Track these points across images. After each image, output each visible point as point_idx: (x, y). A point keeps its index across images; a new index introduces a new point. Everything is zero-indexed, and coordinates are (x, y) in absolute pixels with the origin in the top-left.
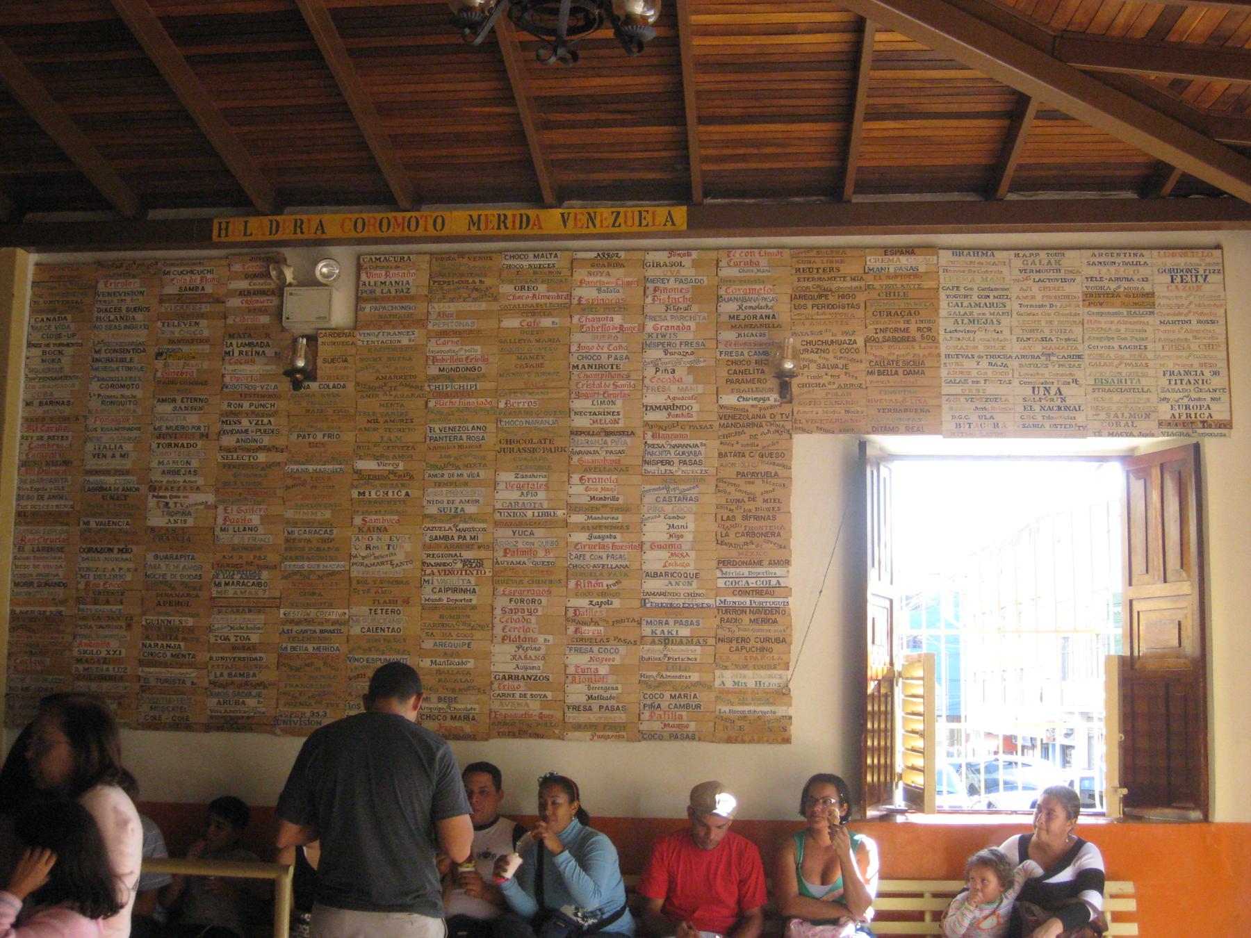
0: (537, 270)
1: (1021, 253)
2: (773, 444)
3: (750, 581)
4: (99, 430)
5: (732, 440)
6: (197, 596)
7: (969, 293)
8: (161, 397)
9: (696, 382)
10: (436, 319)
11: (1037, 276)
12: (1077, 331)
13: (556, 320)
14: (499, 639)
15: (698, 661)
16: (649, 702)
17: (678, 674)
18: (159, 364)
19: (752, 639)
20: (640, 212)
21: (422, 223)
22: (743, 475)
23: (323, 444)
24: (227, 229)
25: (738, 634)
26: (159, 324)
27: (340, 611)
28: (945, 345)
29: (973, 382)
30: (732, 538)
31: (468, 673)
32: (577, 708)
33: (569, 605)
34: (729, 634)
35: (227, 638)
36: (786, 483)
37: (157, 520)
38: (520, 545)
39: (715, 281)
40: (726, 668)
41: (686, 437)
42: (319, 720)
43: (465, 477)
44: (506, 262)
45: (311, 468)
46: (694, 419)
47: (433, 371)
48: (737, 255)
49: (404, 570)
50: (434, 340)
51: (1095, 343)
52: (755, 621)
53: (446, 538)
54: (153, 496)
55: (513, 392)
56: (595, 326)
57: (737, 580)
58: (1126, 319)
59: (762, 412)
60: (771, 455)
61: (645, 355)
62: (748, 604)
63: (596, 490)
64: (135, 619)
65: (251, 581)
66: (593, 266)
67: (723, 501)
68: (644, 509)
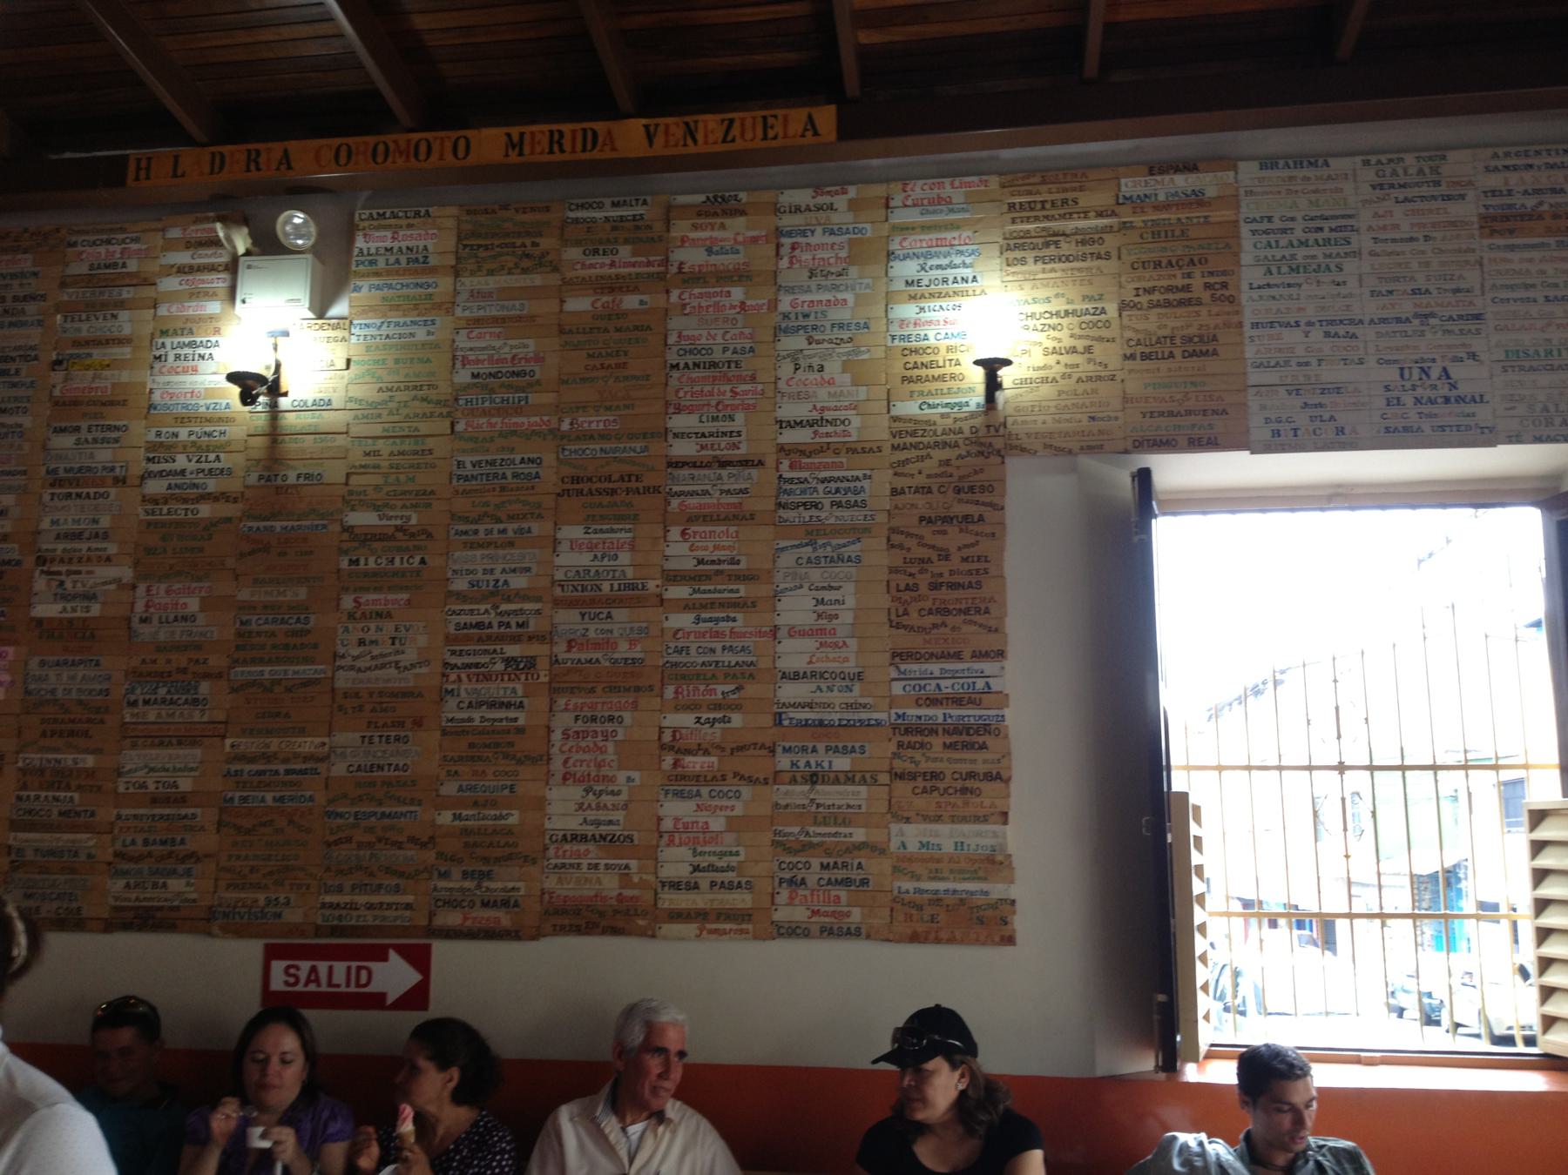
0: (617, 224)
1: (1373, 159)
2: (976, 472)
3: (943, 683)
7: (1290, 225)
8: (58, 425)
10: (467, 300)
11: (1401, 194)
12: (1472, 277)
13: (645, 298)
14: (558, 777)
15: (863, 810)
16: (787, 876)
17: (833, 830)
18: (57, 377)
19: (948, 774)
20: (765, 118)
22: (930, 521)
24: (148, 169)
25: (925, 766)
27: (318, 740)
28: (1252, 306)
29: (1300, 364)
30: (914, 619)
31: (509, 831)
32: (675, 885)
33: (666, 723)
34: (911, 767)
35: (144, 786)
36: (997, 534)
37: (47, 609)
38: (592, 634)
40: (908, 820)
41: (839, 466)
42: (278, 910)
43: (510, 534)
45: (278, 525)
46: (854, 438)
48: (918, 190)
49: (416, 675)
51: (1504, 295)
53: (479, 625)
55: (582, 407)
57: (923, 683)
58: (1555, 254)
59: (959, 424)
60: (971, 489)
61: (779, 346)
62: (940, 720)
63: (706, 549)
65: (184, 697)
66: (699, 215)
67: (899, 563)
68: (779, 577)
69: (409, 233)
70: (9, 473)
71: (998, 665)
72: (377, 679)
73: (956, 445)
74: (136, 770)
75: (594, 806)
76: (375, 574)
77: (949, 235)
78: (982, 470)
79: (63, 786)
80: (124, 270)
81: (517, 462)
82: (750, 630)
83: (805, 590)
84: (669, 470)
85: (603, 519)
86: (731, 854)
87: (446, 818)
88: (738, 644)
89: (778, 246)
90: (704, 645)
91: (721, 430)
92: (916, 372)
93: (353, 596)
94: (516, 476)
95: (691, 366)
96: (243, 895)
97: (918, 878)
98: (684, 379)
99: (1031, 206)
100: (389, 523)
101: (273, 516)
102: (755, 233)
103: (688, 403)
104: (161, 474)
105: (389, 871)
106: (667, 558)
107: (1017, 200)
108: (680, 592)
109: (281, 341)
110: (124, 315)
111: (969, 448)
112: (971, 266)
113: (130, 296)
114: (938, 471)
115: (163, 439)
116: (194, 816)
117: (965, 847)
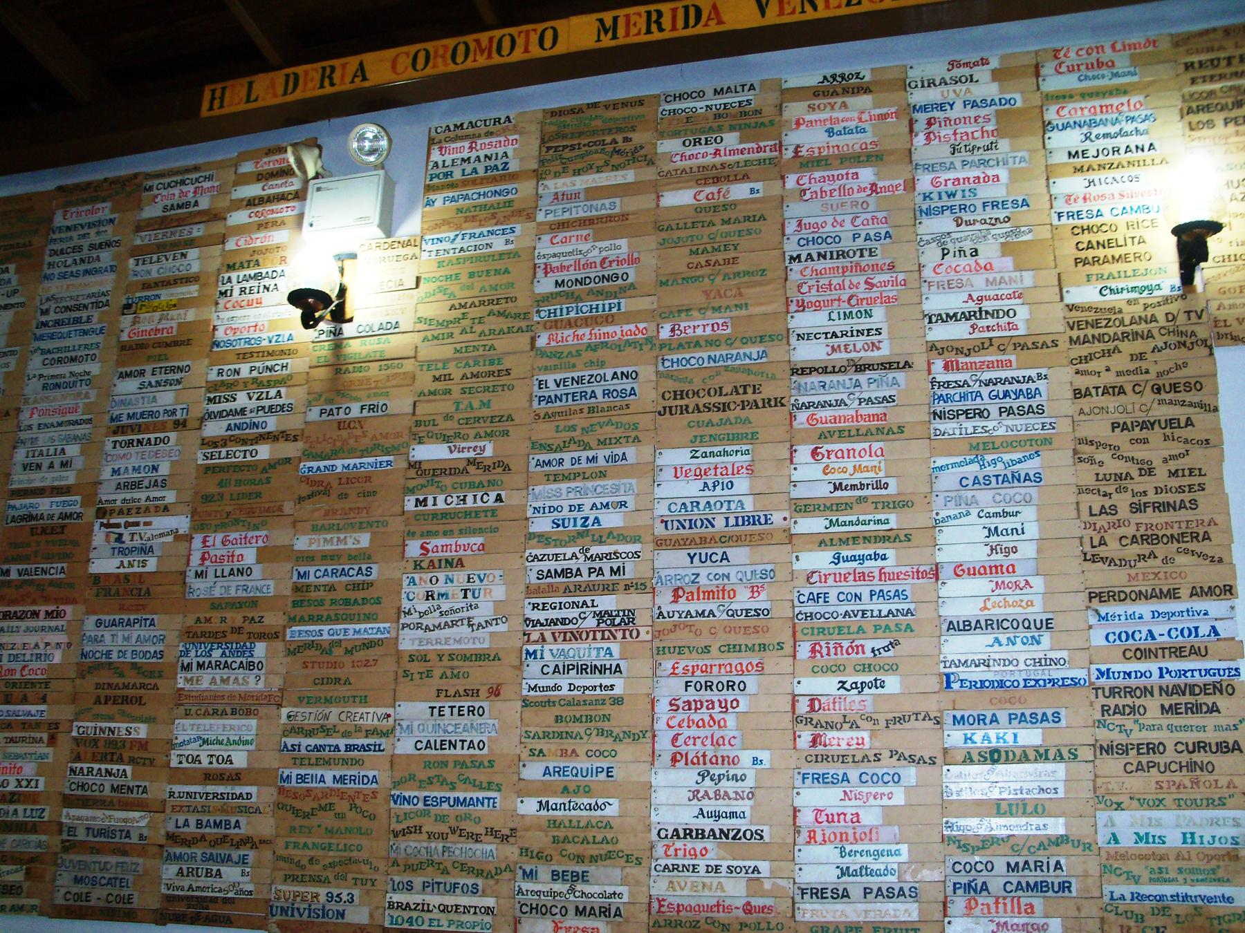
2: (1178, 367)
4: (35, 427)
5: (1093, 365)
6: (156, 687)
9: (1018, 268)
10: (551, 204)
13: (757, 186)
14: (667, 758)
16: (964, 880)
19: (1170, 746)
21: (520, 42)
23: (359, 421)
24: (222, 98)
25: (1138, 736)
26: (131, 261)
27: (381, 711)
30: (1113, 549)
31: (608, 826)
32: (818, 893)
33: (799, 690)
34: (1120, 738)
35: (196, 760)
37: (104, 564)
39: (1036, 100)
43: (601, 462)
44: (668, 107)
45: (339, 464)
47: (546, 285)
49: (492, 634)
50: (546, 238)
52: (1173, 710)
53: (564, 573)
54: (102, 524)
55: (685, 310)
56: (827, 188)
59: (1150, 312)
60: (1174, 387)
64: (61, 728)
65: (238, 660)
67: (1088, 479)
69: (487, 141)
70: (76, 423)
71: (1228, 603)
72: (447, 639)
73: (1150, 335)
74: (189, 742)
75: (712, 795)
76: (445, 514)
77: (1115, 101)
78: (1185, 365)
79: (115, 757)
80: (196, 208)
81: (609, 377)
82: (904, 569)
83: (973, 518)
84: (794, 378)
85: (714, 439)
86: (889, 853)
87: (529, 807)
88: (889, 587)
89: (911, 123)
90: (846, 590)
91: (856, 327)
92: (1090, 254)
93: (420, 542)
94: (606, 393)
95: (815, 256)
96: (302, 889)
97: (1137, 880)
98: (808, 272)
99: (1213, 63)
100: (461, 455)
101: (334, 455)
102: (884, 111)
103: (814, 300)
104: (220, 415)
105: (465, 868)
106: (795, 484)
107: (1195, 59)
108: (813, 525)
109: (348, 264)
110: (193, 253)
111: (1165, 338)
112: (1146, 132)
113: (199, 234)
114: (1132, 366)
115: (225, 377)
116: (249, 795)
117: (1197, 840)
